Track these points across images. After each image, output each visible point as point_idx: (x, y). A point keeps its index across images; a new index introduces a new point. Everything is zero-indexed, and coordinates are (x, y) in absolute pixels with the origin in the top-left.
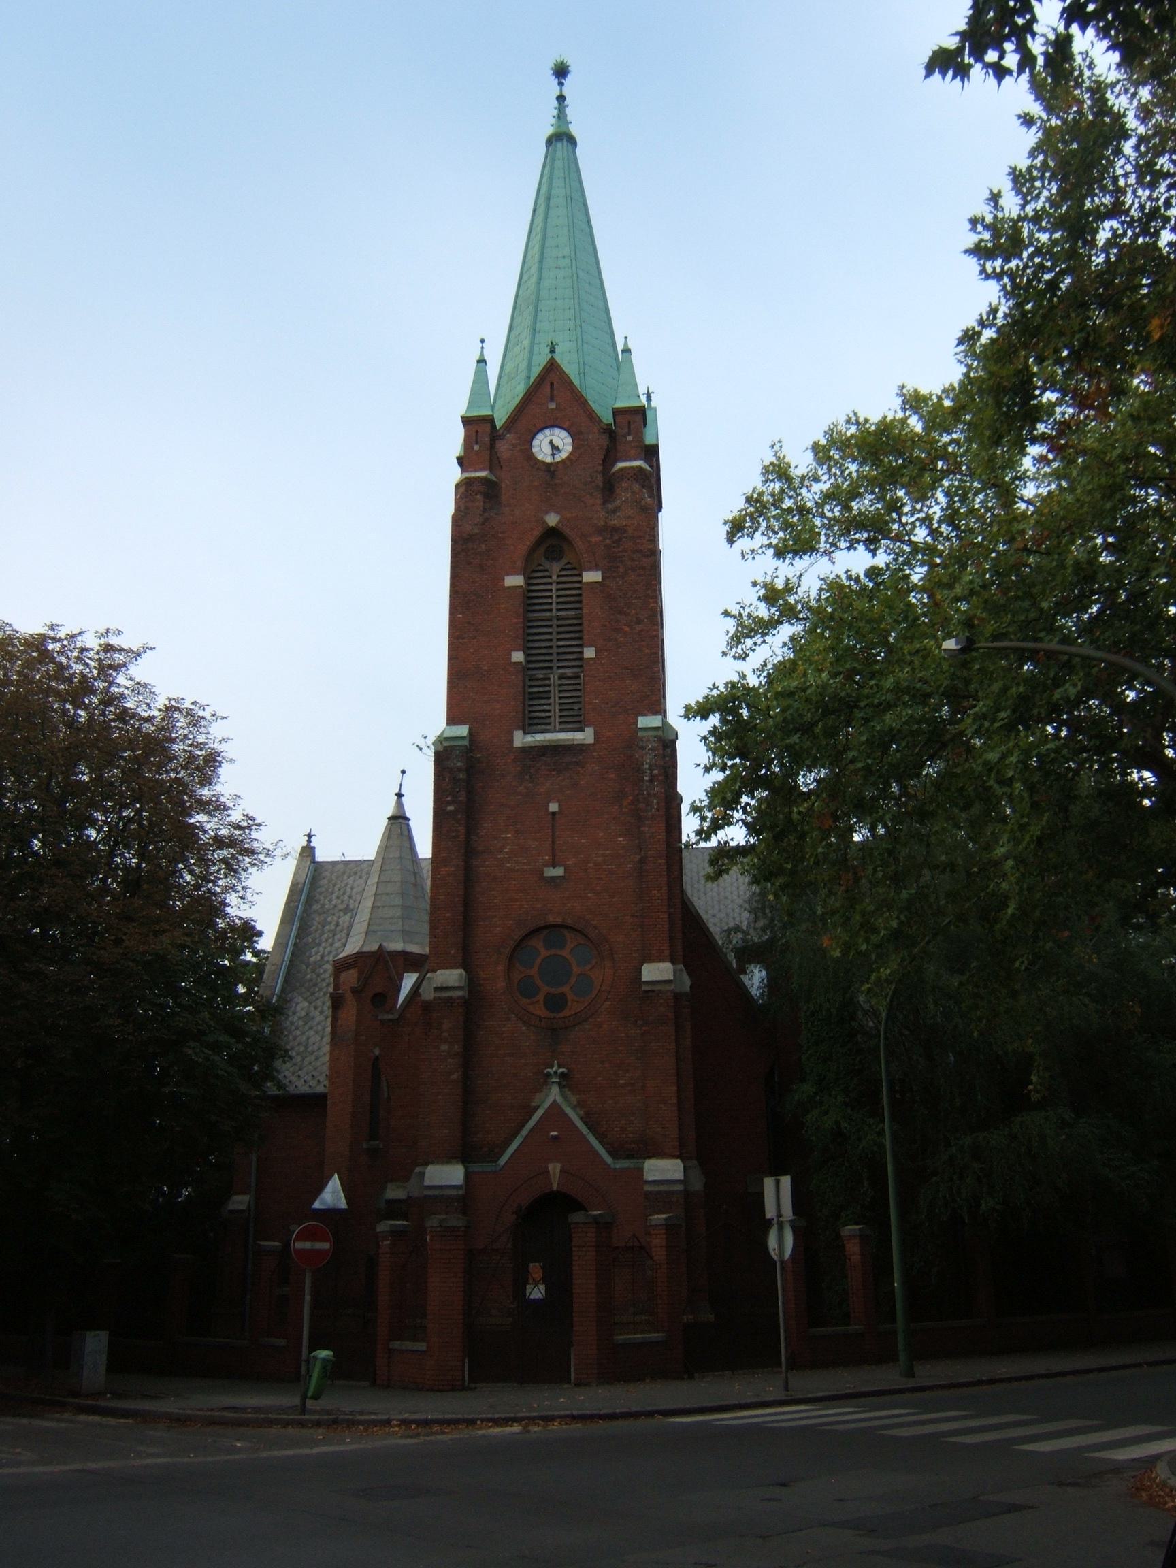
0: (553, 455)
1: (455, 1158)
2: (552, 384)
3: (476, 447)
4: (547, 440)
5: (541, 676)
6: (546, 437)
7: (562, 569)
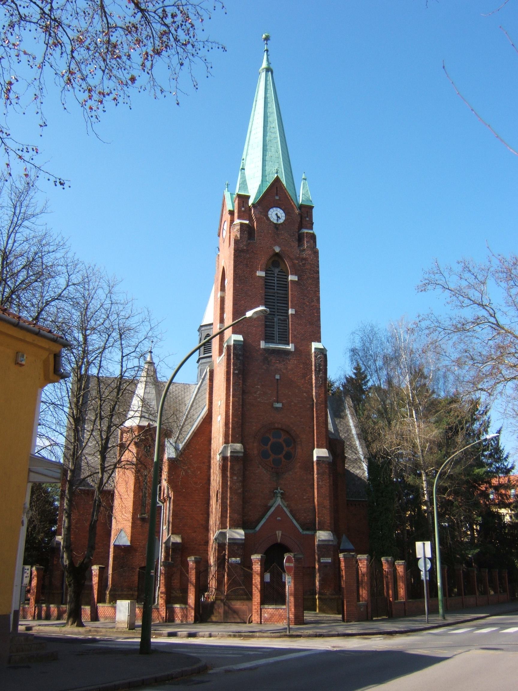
0: (278, 220)
1: (239, 527)
2: (277, 188)
3: (243, 209)
4: (275, 212)
5: (271, 318)
6: (274, 211)
7: (279, 272)
